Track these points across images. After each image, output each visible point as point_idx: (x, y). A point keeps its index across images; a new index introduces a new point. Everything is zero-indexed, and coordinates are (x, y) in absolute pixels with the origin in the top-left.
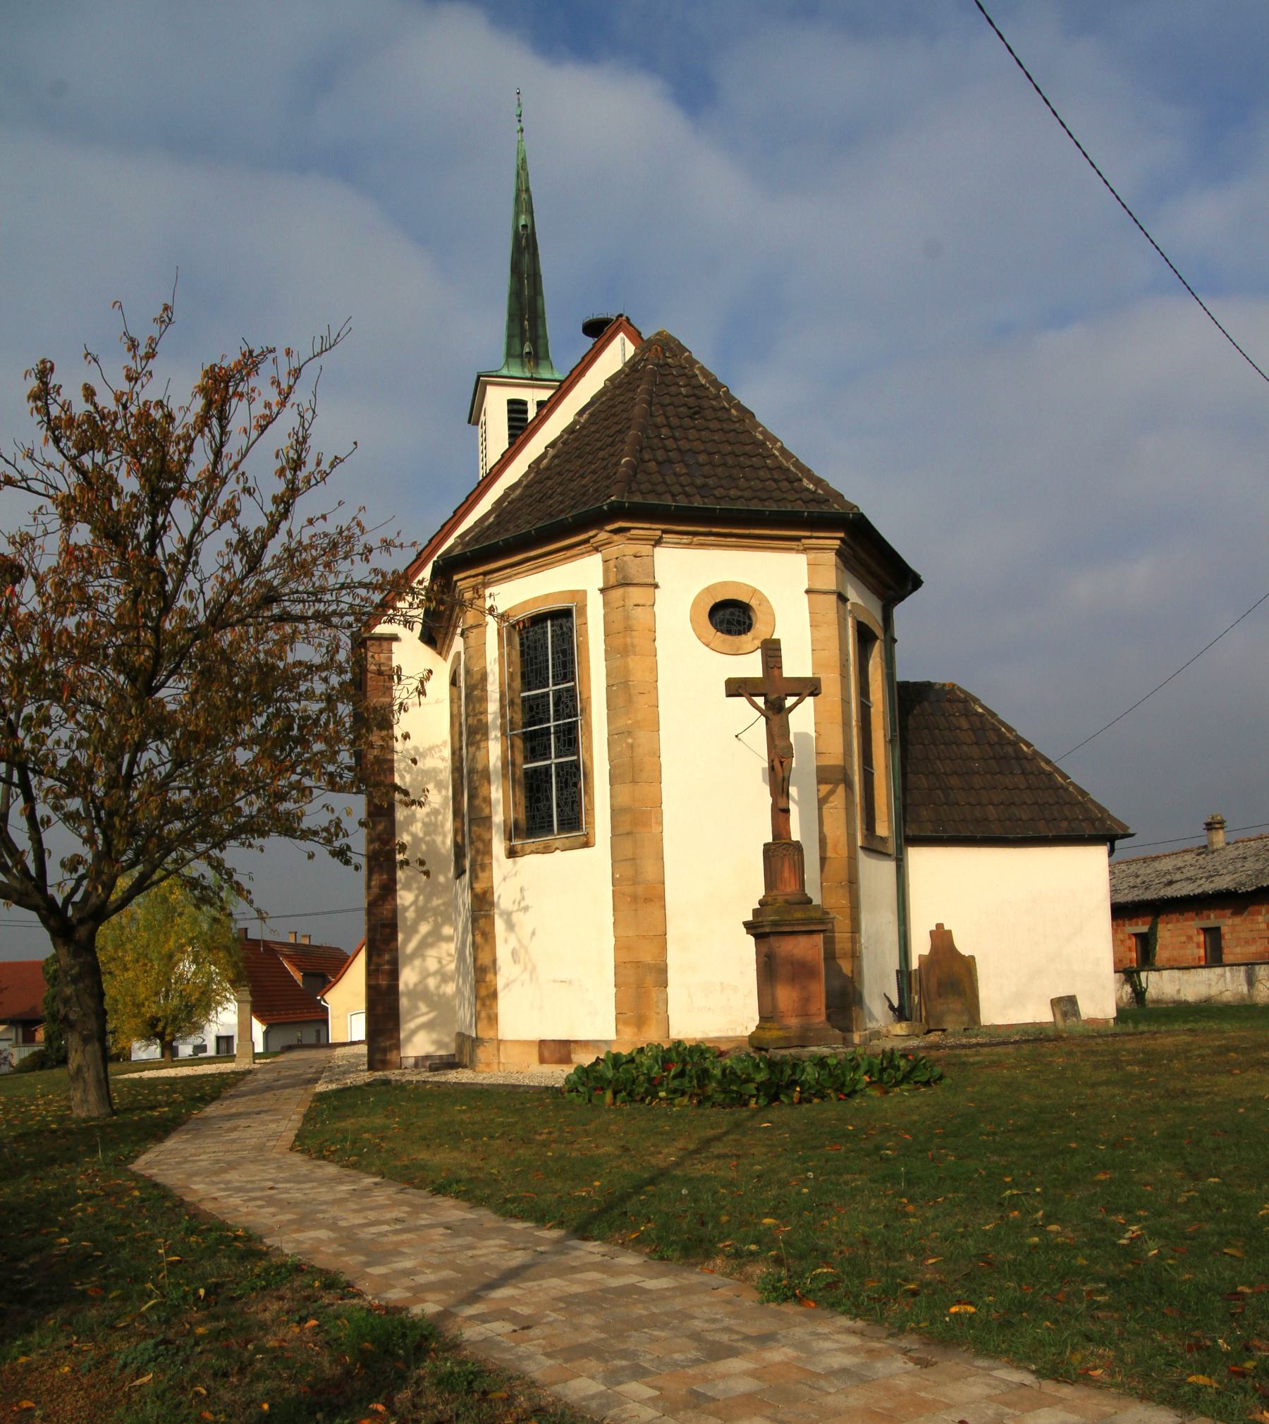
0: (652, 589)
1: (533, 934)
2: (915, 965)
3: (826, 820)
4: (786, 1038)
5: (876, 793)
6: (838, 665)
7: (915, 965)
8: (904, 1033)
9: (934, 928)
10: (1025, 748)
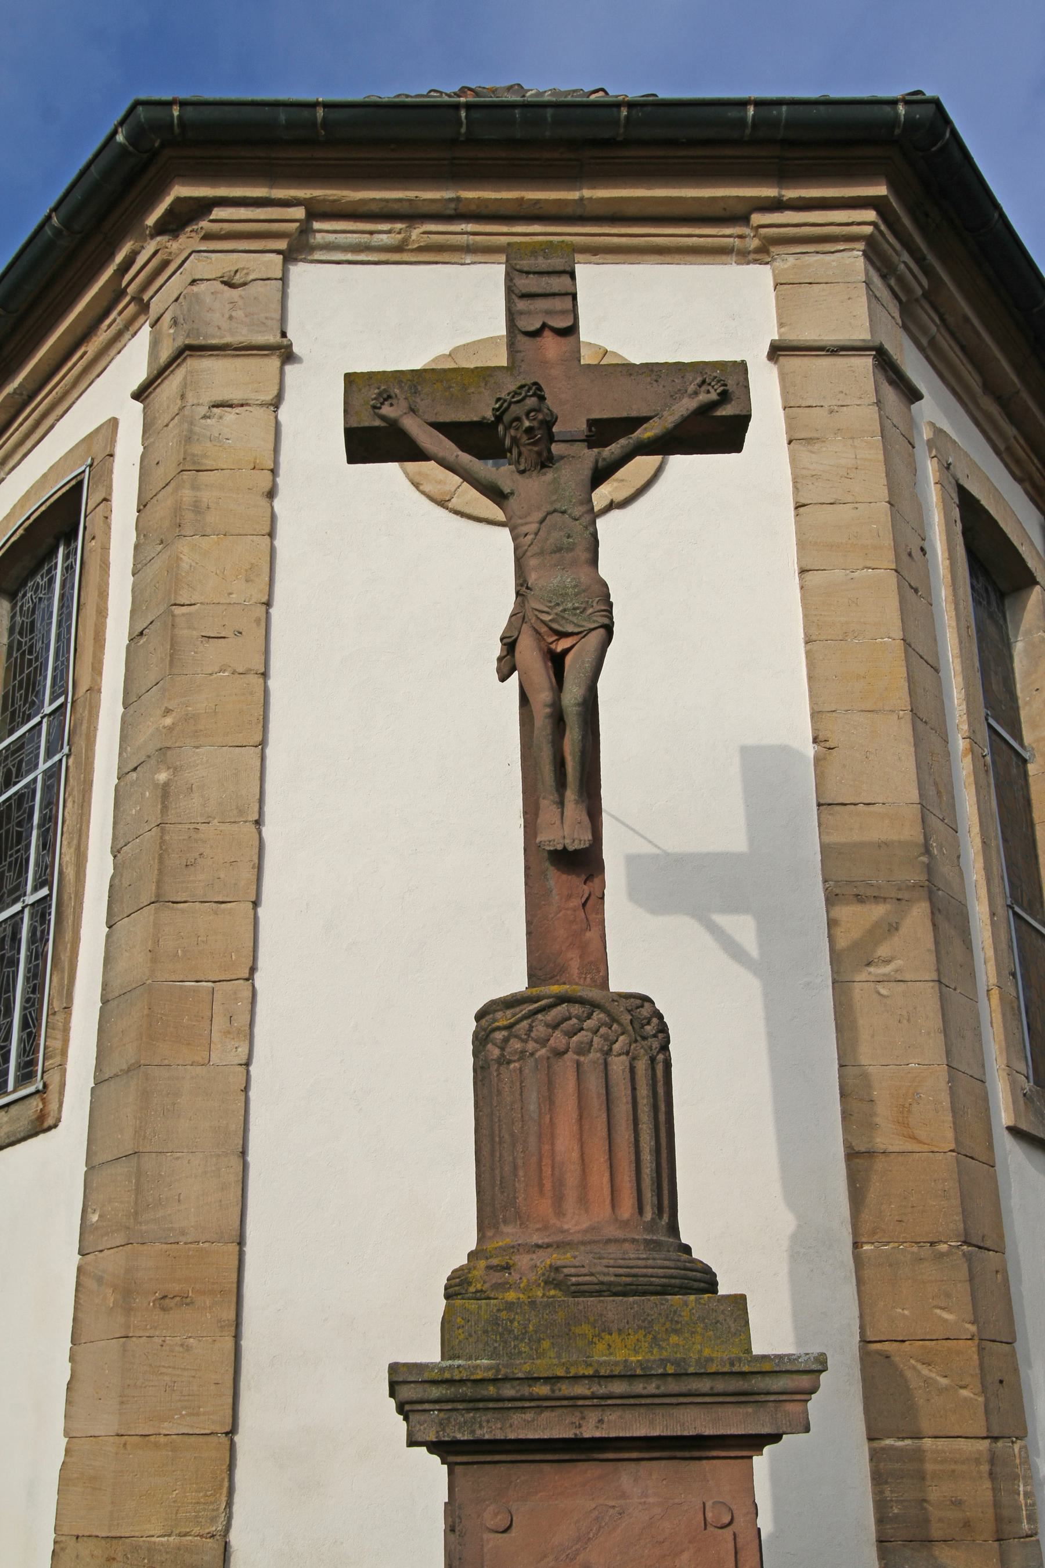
0: (274, 362)
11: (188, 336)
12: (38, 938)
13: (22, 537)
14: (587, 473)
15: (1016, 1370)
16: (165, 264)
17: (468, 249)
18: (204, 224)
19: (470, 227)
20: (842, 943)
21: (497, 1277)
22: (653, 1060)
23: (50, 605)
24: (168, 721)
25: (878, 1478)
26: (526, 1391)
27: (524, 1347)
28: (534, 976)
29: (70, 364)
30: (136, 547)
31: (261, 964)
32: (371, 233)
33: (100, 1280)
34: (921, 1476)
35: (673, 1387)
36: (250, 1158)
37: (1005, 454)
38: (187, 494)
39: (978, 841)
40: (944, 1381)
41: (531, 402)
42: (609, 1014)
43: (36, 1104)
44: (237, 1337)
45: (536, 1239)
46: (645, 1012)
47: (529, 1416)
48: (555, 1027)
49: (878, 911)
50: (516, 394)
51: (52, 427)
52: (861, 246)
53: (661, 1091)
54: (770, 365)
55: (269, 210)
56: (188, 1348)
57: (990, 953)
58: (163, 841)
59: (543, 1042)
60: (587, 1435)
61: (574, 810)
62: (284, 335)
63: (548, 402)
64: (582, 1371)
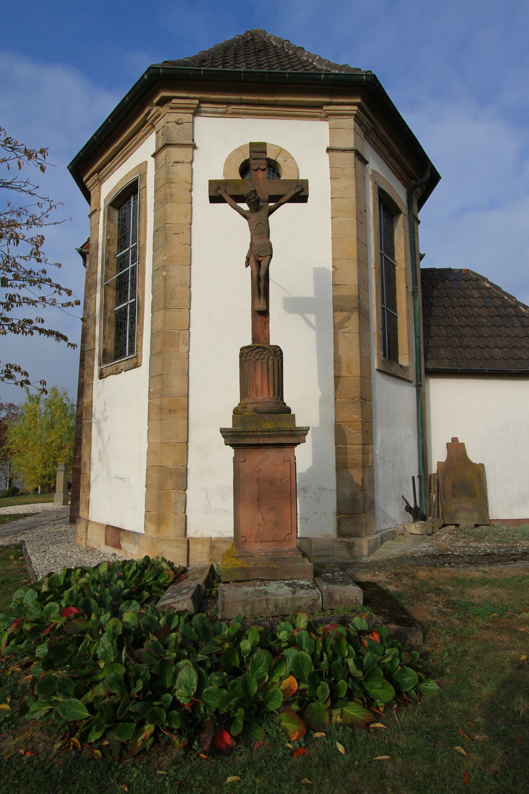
0: (190, 149)
1: (109, 439)
2: (434, 469)
3: (341, 343)
4: (242, 569)
5: (399, 332)
6: (355, 210)
7: (434, 469)
8: (418, 533)
9: (450, 441)
10: (523, 310)
11: (167, 140)
12: (133, 314)
13: (121, 193)
14: (267, 213)
15: (372, 429)
16: (159, 115)
17: (245, 114)
18: (170, 104)
19: (245, 107)
20: (336, 322)
21: (243, 410)
22: (278, 361)
23: (130, 214)
24: (165, 258)
25: (337, 454)
26: (248, 434)
27: (248, 425)
28: (253, 343)
29: (133, 140)
30: (154, 204)
31: (191, 325)
32: (217, 108)
33: (154, 406)
34: (346, 453)
35: (278, 433)
36: (190, 376)
37: (396, 173)
38: (168, 190)
39: (375, 293)
40: (353, 432)
41: (254, 195)
42: (269, 351)
43: (135, 360)
44: (188, 420)
45: (252, 401)
46: (277, 350)
47: (249, 439)
48: (257, 354)
49: (345, 314)
50: (250, 193)
51: (128, 158)
52: (353, 117)
53: (280, 368)
54: (327, 154)
55: (188, 100)
56: (176, 423)
57: (376, 324)
58: (165, 292)
59: (254, 357)
60: (260, 443)
61: (262, 301)
62: (193, 141)
63: (258, 195)
64: (259, 430)
